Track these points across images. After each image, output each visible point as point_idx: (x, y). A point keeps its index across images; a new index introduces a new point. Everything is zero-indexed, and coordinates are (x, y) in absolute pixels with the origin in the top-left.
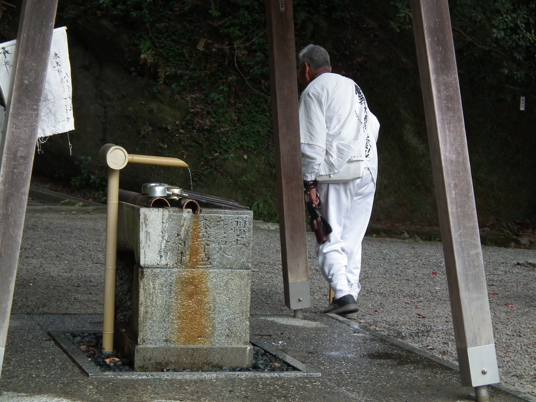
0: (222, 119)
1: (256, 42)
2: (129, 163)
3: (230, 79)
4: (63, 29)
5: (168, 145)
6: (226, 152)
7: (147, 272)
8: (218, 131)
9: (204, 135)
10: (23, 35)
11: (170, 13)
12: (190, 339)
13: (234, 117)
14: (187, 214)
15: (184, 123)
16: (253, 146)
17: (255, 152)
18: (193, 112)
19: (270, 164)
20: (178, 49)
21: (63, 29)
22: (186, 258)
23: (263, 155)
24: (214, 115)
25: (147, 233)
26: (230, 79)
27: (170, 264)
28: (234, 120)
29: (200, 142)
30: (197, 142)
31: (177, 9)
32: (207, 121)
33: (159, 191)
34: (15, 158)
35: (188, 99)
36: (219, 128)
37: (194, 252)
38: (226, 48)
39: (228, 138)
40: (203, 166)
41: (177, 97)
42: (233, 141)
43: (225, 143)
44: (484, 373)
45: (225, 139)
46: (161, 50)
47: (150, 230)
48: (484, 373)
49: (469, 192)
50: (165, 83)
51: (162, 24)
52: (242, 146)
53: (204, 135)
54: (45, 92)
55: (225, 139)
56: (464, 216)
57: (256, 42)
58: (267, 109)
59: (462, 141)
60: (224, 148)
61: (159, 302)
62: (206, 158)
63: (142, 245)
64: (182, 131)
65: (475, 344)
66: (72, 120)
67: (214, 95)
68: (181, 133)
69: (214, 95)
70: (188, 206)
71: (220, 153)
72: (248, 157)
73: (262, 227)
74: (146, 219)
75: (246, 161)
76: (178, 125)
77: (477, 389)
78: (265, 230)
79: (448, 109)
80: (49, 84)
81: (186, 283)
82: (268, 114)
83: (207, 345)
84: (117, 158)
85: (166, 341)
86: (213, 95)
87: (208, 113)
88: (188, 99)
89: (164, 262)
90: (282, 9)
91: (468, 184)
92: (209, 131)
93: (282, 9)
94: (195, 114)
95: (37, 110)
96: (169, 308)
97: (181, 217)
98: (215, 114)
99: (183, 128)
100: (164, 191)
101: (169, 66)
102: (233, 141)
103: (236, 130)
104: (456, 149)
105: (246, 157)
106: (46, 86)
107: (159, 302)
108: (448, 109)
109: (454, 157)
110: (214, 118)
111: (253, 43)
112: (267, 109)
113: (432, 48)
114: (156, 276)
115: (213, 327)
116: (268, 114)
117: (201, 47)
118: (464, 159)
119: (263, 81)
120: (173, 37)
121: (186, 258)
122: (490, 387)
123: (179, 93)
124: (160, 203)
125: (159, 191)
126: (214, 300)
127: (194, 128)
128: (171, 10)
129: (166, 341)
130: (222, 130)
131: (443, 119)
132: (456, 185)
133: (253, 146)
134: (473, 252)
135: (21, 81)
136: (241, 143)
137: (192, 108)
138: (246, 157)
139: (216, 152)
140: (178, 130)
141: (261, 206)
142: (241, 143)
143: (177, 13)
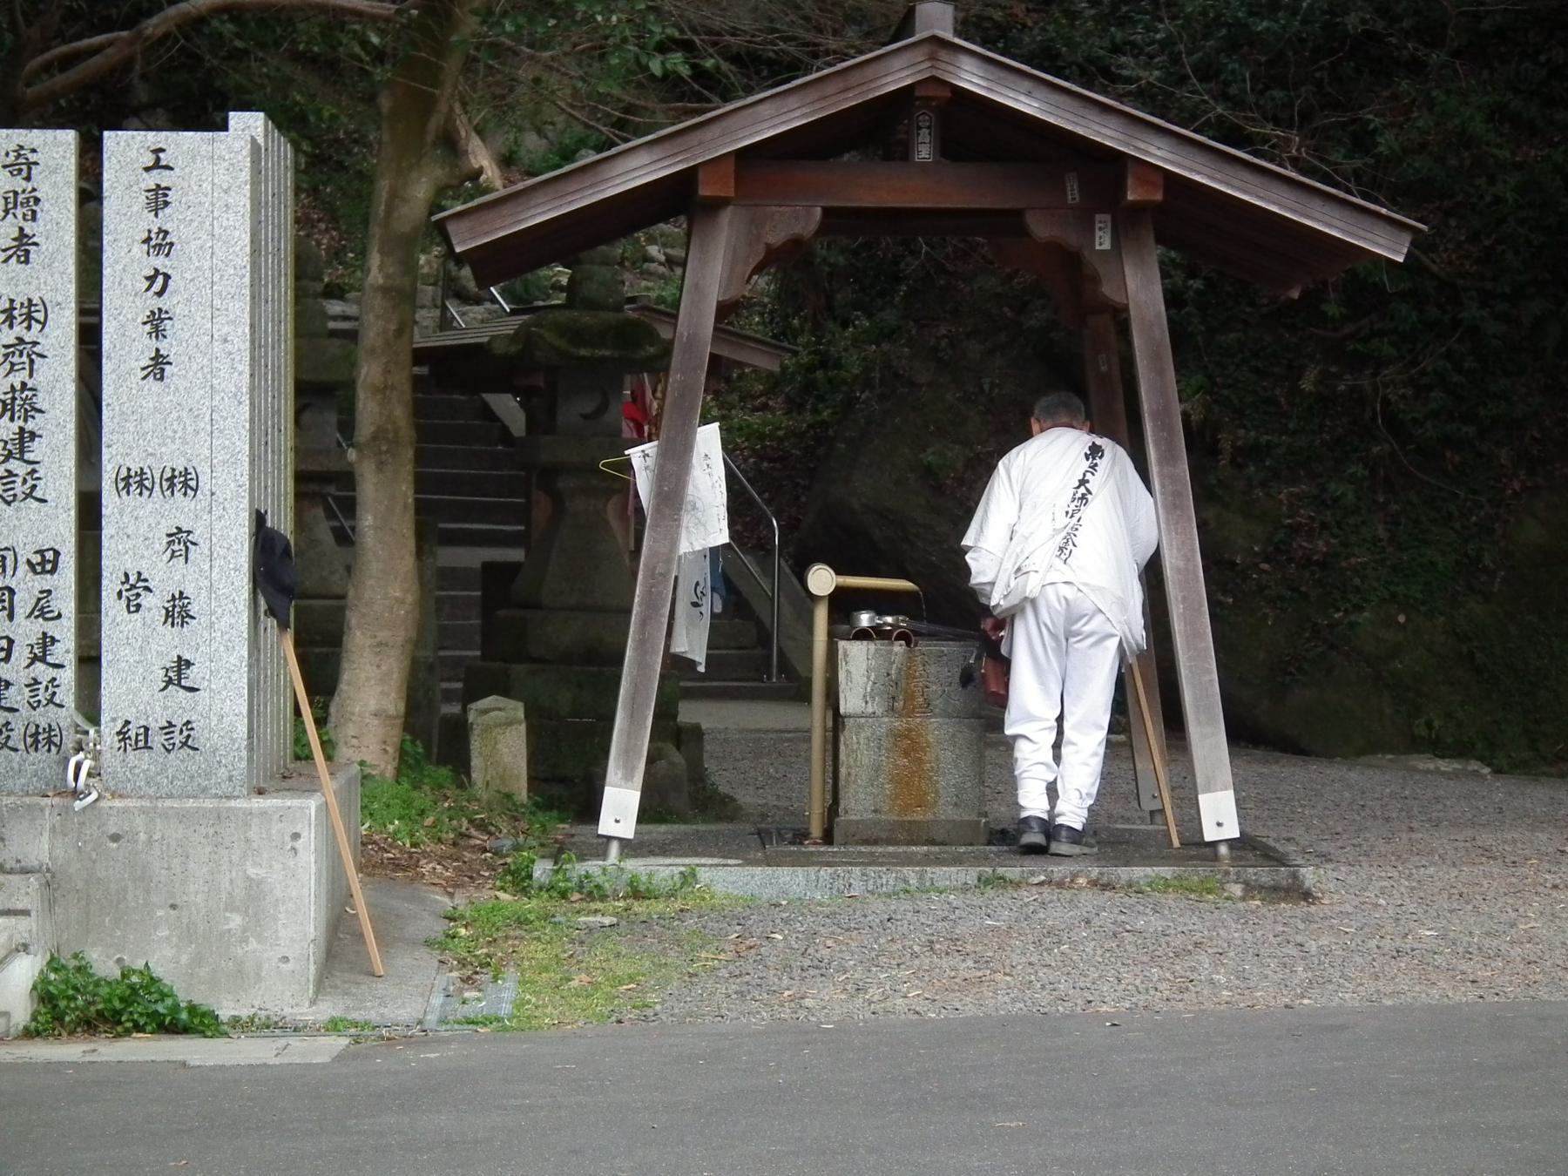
0: (1353, 538)
1: (1429, 369)
2: (837, 588)
3: (1376, 450)
4: (714, 427)
5: (1234, 597)
6: (1359, 608)
7: (849, 723)
8: (1344, 564)
9: (1313, 573)
10: (663, 435)
11: (1248, 309)
12: (905, 808)
13: (1382, 533)
14: (899, 648)
15: (1271, 548)
16: (1419, 596)
17: (1423, 609)
18: (1290, 526)
19: (1457, 634)
20: (1264, 388)
21: (714, 427)
22: (899, 705)
23: (1441, 614)
24: (1336, 531)
25: (848, 672)
26: (1376, 450)
27: (879, 711)
28: (1381, 540)
29: (1303, 589)
30: (1295, 590)
31: (1265, 301)
32: (1320, 543)
33: (865, 619)
34: (653, 576)
35: (1282, 496)
36: (1347, 558)
37: (909, 697)
38: (1366, 384)
39: (1364, 578)
40: (1308, 640)
41: (1258, 492)
42: (1376, 584)
43: (1357, 590)
44: (1219, 825)
45: (1357, 581)
46: (1226, 392)
47: (852, 670)
48: (1219, 825)
49: (1201, 606)
50: (1233, 462)
51: (1233, 335)
52: (1394, 596)
53: (1313, 573)
54: (690, 498)
55: (1357, 581)
56: (1194, 635)
57: (1429, 369)
58: (1456, 514)
59: (1193, 545)
60: (1355, 601)
61: (866, 761)
62: (1316, 624)
63: (841, 688)
64: (1265, 566)
65: (1208, 790)
66: (726, 531)
67: (1336, 489)
68: (1265, 571)
69: (1336, 489)
70: (898, 638)
71: (1346, 611)
72: (1408, 620)
73: (1421, 766)
74: (846, 654)
75: (1403, 627)
76: (1257, 554)
77: (1214, 844)
78: (1428, 772)
79: (1175, 506)
80: (696, 487)
81: (897, 736)
82: (1458, 526)
83: (930, 816)
84: (822, 580)
85: (875, 811)
86: (1332, 486)
87: (1324, 526)
88: (1282, 496)
89: (870, 709)
90: (1104, 368)
91: (1200, 596)
92: (1323, 565)
93: (1104, 368)
94: (1295, 530)
95: (679, 520)
96: (878, 769)
97: (890, 652)
98: (1340, 528)
99: (1267, 561)
100: (872, 619)
101: (1245, 427)
102: (1376, 584)
103: (1383, 560)
104: (1185, 555)
105: (1402, 619)
106: (690, 489)
107: (866, 761)
108: (1175, 506)
109: (1182, 564)
110: (1336, 537)
111: (1423, 373)
112: (1456, 514)
113: (1154, 434)
114: (860, 727)
115: (937, 792)
116: (1458, 526)
117: (1307, 385)
118: (1196, 566)
119: (1448, 454)
120: (1253, 363)
121: (899, 705)
122: (1230, 842)
123: (1263, 485)
124: (863, 635)
125: (865, 619)
126: (937, 759)
127: (1290, 560)
128: (1252, 304)
129: (875, 811)
130: (1353, 561)
131: (1167, 519)
132: (1184, 598)
133: (1419, 596)
134: (1206, 678)
135: (660, 487)
136: (1392, 588)
137: (1290, 517)
138: (1402, 619)
139: (1338, 610)
140: (1256, 565)
141: (1436, 724)
142: (1392, 588)
143: (1265, 310)
